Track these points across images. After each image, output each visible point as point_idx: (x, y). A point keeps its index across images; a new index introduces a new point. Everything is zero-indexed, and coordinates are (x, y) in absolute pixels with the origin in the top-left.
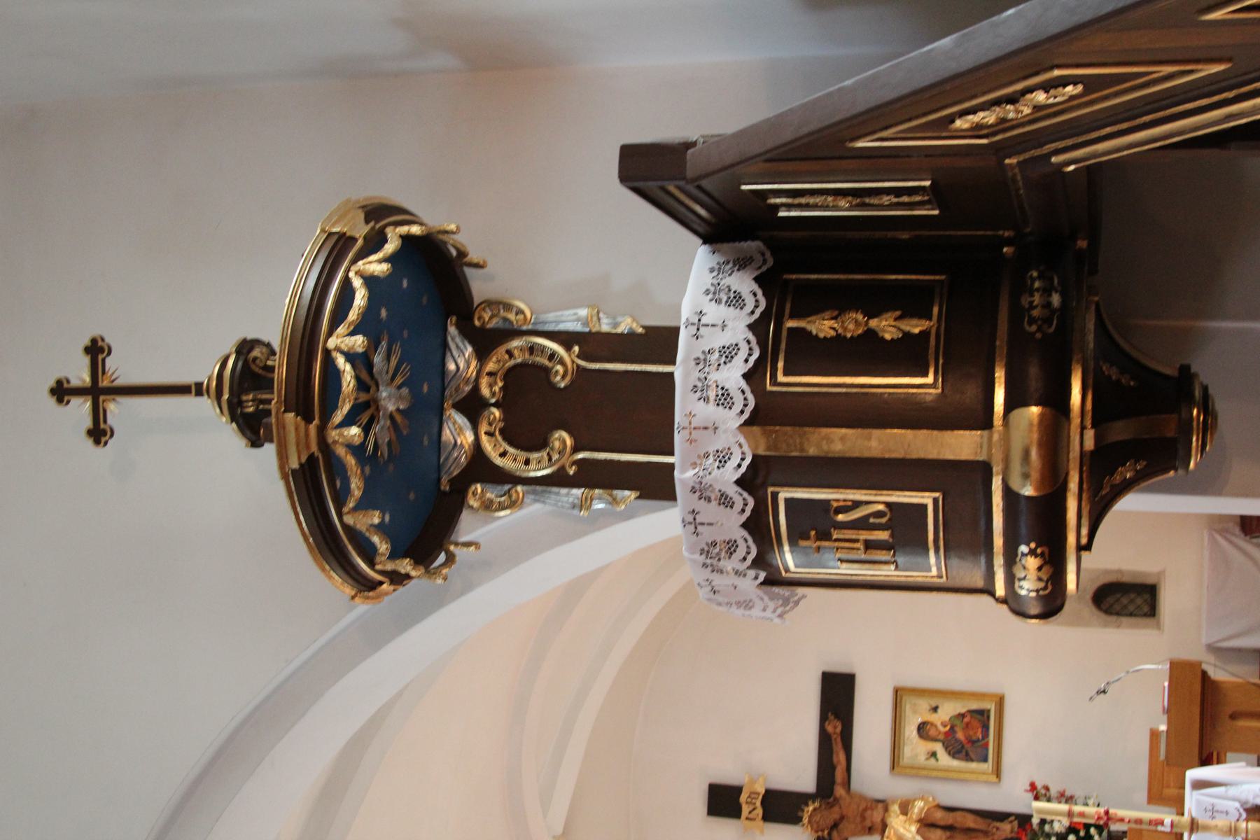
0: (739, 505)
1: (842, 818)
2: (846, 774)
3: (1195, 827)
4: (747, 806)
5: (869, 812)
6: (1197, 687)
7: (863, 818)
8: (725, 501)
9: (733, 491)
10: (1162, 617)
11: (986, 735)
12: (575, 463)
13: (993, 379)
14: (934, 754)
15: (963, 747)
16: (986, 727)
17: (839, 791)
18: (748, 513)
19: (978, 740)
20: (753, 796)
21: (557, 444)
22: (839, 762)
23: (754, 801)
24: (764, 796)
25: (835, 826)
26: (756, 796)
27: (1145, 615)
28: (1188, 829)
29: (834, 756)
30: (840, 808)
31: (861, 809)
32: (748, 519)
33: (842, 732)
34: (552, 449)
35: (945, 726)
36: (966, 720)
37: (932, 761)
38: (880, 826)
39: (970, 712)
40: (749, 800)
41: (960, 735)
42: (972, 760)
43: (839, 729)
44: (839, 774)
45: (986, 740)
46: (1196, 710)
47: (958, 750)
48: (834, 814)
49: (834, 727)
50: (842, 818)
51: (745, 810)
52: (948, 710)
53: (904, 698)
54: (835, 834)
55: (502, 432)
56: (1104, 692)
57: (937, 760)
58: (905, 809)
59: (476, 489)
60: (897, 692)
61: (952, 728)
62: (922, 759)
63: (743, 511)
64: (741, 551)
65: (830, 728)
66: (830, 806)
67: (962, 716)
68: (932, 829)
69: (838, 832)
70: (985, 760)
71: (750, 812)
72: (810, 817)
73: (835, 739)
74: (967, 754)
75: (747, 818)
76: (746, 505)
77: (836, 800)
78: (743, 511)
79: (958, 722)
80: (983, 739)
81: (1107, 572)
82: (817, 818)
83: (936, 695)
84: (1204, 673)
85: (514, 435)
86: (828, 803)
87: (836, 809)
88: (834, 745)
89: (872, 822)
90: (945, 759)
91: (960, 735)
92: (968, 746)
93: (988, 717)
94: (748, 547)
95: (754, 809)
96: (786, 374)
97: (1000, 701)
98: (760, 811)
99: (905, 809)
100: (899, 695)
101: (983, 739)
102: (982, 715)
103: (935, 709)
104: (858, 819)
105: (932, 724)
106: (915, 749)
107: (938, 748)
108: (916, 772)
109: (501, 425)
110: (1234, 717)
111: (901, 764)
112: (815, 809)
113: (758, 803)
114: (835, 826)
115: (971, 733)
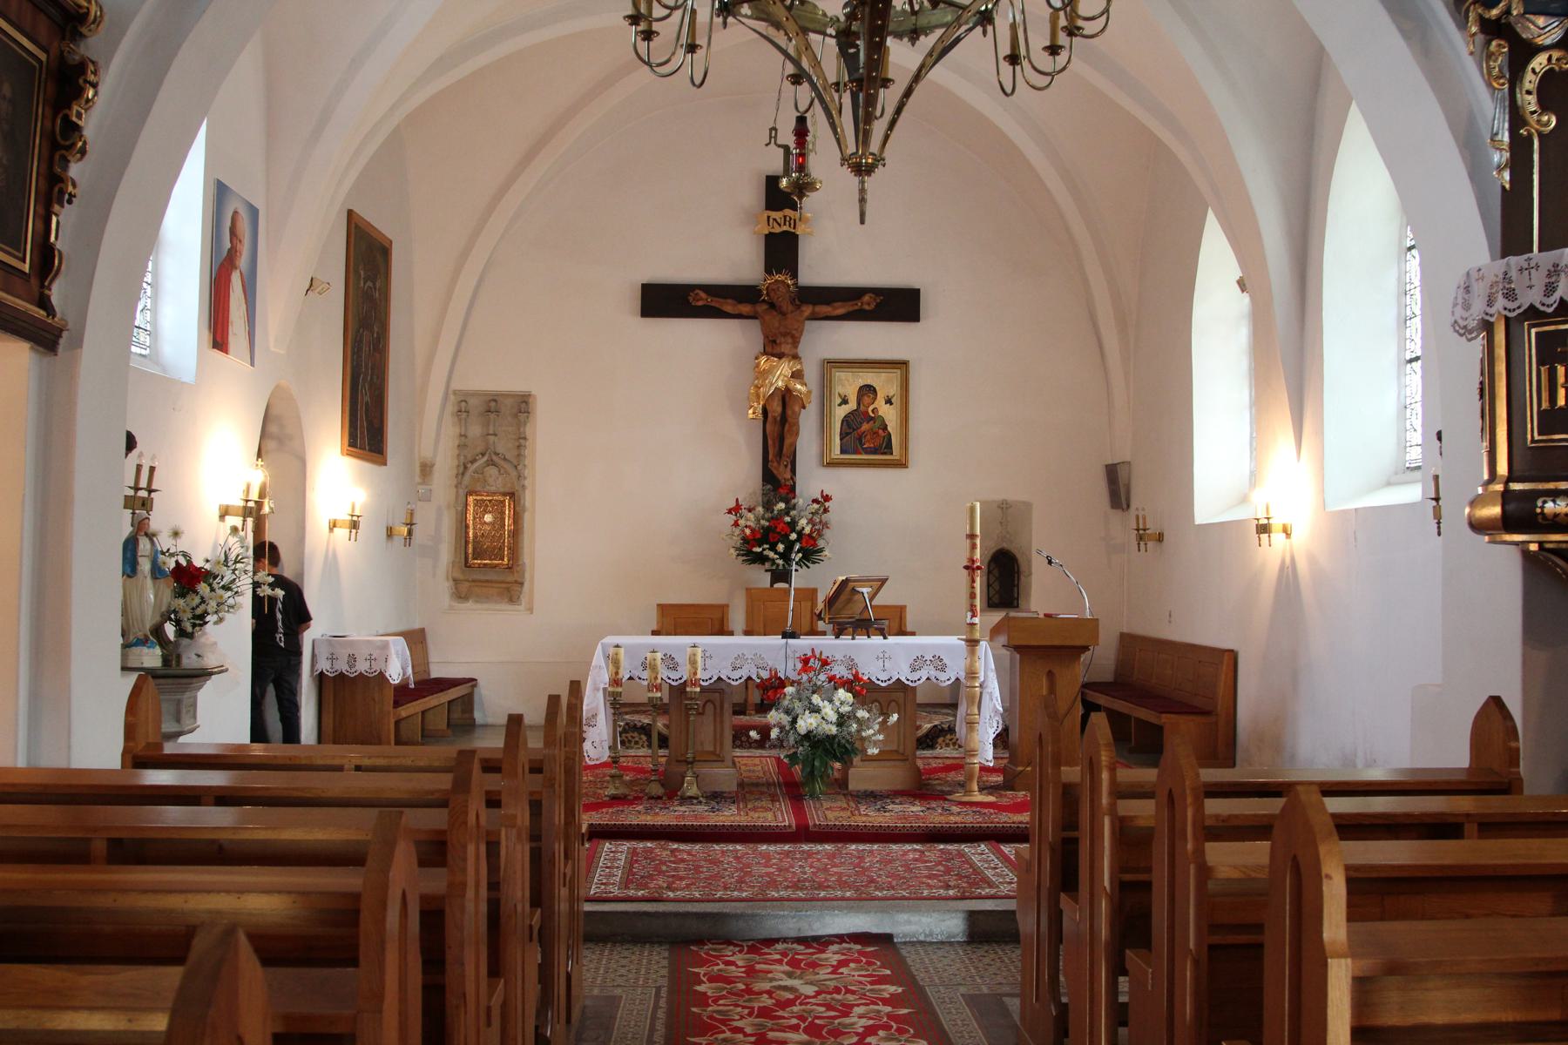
0: (1550, 301)
1: (784, 314)
2: (821, 316)
3: (973, 644)
4: (781, 216)
5: (790, 340)
6: (1079, 642)
7: (785, 335)
8: (1550, 289)
9: (1557, 296)
10: (989, 614)
11: (867, 451)
12: (1530, 137)
13: (1524, 482)
14: (845, 401)
15: (854, 430)
16: (875, 451)
17: (807, 310)
18: (1542, 308)
19: (862, 444)
20: (792, 222)
21: (1546, 118)
22: (837, 308)
23: (787, 223)
24: (794, 233)
25: (772, 306)
26: (792, 226)
27: (989, 599)
28: (969, 637)
29: (839, 304)
30: (792, 312)
31: (794, 332)
32: (1538, 309)
33: (865, 311)
34: (1540, 114)
35: (873, 411)
36: (881, 431)
37: (839, 401)
38: (777, 350)
39: (889, 434)
40: (788, 219)
41: (865, 427)
42: (841, 439)
43: (866, 307)
44: (824, 309)
45: (861, 451)
46: (1056, 642)
47: (851, 424)
48: (787, 306)
49: (867, 302)
50: (784, 314)
51: (777, 215)
52: (889, 414)
53: (899, 371)
54: (765, 307)
55: (1552, 70)
56: (1050, 562)
57: (840, 405)
58: (797, 375)
59: (1504, 47)
60: (906, 363)
61: (872, 418)
62: (839, 389)
63: (1543, 305)
64: (1511, 305)
65: (866, 298)
66: (792, 301)
67: (885, 428)
68: (781, 403)
69: (767, 309)
70: (843, 451)
71: (775, 220)
72: (783, 282)
73: (857, 304)
74: (847, 434)
75: (769, 217)
76: (1548, 306)
77: (798, 307)
78: (1543, 305)
79: (877, 424)
80: (863, 449)
81: (1029, 562)
82: (782, 289)
83: (904, 401)
84: (1086, 648)
85: (1549, 80)
86: (794, 299)
87: (791, 308)
88: (851, 303)
89: (780, 344)
90: (841, 412)
91: (865, 427)
92: (855, 434)
93: (885, 453)
94: (1514, 310)
95: (780, 225)
96: (1537, 333)
97: (902, 464)
98: (777, 230)
99: (797, 375)
100: (902, 365)
101: (863, 449)
102: (888, 448)
103: (889, 401)
104: (782, 330)
105: (875, 399)
106: (849, 384)
107: (852, 405)
108: (826, 385)
109: (1557, 68)
110: (1050, 674)
111: (833, 370)
112: (788, 286)
113: (785, 228)
114: (772, 306)
115: (868, 437)
